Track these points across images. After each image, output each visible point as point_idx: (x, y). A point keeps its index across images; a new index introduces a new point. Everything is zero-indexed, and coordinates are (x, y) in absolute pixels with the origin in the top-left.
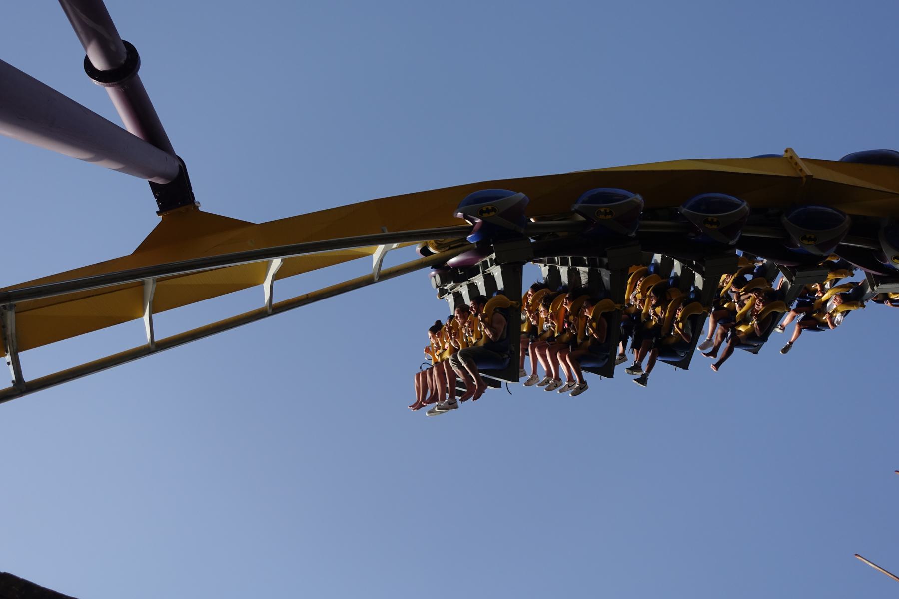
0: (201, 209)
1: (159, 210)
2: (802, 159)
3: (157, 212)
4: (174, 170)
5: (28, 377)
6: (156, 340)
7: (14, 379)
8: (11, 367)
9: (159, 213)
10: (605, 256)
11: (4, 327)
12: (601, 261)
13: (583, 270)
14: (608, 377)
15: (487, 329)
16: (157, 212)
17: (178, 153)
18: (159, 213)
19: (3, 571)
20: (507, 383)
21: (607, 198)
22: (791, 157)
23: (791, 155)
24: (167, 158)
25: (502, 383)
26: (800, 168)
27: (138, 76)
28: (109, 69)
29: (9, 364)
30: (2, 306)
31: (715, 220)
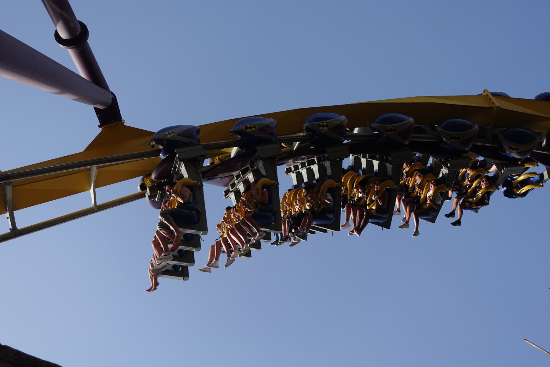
0: (125, 124)
1: (100, 124)
3: (99, 126)
4: (110, 100)
5: (19, 226)
6: (97, 204)
7: (11, 227)
8: (9, 220)
9: (100, 126)
11: (5, 195)
12: (324, 156)
13: (376, 163)
15: (178, 197)
16: (99, 126)
18: (100, 126)
19: (3, 344)
20: (332, 232)
21: (391, 120)
22: (487, 95)
23: (487, 94)
24: (104, 93)
26: (492, 102)
27: (88, 43)
28: (70, 38)
29: (8, 218)
30: (4, 183)
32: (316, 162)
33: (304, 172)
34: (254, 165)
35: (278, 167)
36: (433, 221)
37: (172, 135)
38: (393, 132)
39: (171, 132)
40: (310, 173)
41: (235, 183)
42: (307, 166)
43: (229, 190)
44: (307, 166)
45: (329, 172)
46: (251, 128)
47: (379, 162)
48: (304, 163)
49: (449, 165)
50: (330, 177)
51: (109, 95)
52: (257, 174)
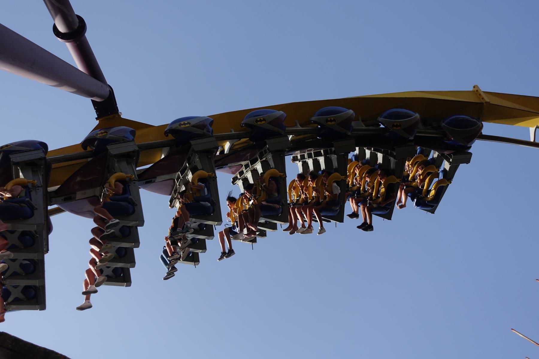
0: (122, 117)
1: (97, 117)
2: (483, 92)
3: (96, 118)
4: (106, 92)
10: (333, 147)
12: (331, 150)
13: (380, 156)
14: (340, 222)
16: (96, 118)
17: (109, 83)
19: (1, 331)
22: (477, 91)
23: (477, 89)
25: (277, 224)
31: (332, 119)
32: (323, 154)
33: (310, 162)
34: (263, 157)
35: (286, 157)
36: (433, 213)
37: (187, 126)
38: (399, 128)
39: (186, 122)
40: (316, 163)
41: (243, 171)
42: (313, 157)
43: (237, 177)
44: (313, 157)
45: (335, 164)
46: (261, 121)
47: (383, 155)
48: (311, 153)
49: (451, 160)
50: (336, 170)
51: (106, 88)
52: (265, 165)
